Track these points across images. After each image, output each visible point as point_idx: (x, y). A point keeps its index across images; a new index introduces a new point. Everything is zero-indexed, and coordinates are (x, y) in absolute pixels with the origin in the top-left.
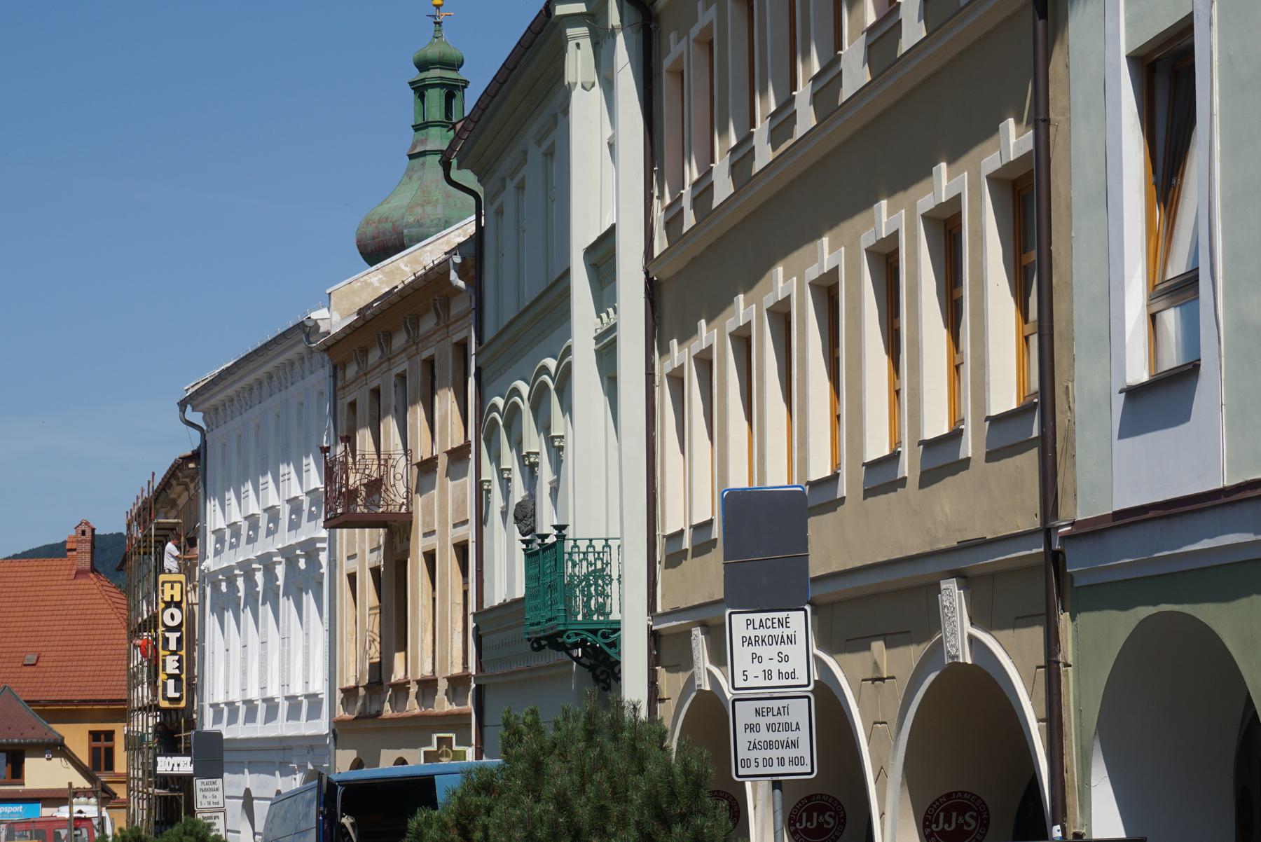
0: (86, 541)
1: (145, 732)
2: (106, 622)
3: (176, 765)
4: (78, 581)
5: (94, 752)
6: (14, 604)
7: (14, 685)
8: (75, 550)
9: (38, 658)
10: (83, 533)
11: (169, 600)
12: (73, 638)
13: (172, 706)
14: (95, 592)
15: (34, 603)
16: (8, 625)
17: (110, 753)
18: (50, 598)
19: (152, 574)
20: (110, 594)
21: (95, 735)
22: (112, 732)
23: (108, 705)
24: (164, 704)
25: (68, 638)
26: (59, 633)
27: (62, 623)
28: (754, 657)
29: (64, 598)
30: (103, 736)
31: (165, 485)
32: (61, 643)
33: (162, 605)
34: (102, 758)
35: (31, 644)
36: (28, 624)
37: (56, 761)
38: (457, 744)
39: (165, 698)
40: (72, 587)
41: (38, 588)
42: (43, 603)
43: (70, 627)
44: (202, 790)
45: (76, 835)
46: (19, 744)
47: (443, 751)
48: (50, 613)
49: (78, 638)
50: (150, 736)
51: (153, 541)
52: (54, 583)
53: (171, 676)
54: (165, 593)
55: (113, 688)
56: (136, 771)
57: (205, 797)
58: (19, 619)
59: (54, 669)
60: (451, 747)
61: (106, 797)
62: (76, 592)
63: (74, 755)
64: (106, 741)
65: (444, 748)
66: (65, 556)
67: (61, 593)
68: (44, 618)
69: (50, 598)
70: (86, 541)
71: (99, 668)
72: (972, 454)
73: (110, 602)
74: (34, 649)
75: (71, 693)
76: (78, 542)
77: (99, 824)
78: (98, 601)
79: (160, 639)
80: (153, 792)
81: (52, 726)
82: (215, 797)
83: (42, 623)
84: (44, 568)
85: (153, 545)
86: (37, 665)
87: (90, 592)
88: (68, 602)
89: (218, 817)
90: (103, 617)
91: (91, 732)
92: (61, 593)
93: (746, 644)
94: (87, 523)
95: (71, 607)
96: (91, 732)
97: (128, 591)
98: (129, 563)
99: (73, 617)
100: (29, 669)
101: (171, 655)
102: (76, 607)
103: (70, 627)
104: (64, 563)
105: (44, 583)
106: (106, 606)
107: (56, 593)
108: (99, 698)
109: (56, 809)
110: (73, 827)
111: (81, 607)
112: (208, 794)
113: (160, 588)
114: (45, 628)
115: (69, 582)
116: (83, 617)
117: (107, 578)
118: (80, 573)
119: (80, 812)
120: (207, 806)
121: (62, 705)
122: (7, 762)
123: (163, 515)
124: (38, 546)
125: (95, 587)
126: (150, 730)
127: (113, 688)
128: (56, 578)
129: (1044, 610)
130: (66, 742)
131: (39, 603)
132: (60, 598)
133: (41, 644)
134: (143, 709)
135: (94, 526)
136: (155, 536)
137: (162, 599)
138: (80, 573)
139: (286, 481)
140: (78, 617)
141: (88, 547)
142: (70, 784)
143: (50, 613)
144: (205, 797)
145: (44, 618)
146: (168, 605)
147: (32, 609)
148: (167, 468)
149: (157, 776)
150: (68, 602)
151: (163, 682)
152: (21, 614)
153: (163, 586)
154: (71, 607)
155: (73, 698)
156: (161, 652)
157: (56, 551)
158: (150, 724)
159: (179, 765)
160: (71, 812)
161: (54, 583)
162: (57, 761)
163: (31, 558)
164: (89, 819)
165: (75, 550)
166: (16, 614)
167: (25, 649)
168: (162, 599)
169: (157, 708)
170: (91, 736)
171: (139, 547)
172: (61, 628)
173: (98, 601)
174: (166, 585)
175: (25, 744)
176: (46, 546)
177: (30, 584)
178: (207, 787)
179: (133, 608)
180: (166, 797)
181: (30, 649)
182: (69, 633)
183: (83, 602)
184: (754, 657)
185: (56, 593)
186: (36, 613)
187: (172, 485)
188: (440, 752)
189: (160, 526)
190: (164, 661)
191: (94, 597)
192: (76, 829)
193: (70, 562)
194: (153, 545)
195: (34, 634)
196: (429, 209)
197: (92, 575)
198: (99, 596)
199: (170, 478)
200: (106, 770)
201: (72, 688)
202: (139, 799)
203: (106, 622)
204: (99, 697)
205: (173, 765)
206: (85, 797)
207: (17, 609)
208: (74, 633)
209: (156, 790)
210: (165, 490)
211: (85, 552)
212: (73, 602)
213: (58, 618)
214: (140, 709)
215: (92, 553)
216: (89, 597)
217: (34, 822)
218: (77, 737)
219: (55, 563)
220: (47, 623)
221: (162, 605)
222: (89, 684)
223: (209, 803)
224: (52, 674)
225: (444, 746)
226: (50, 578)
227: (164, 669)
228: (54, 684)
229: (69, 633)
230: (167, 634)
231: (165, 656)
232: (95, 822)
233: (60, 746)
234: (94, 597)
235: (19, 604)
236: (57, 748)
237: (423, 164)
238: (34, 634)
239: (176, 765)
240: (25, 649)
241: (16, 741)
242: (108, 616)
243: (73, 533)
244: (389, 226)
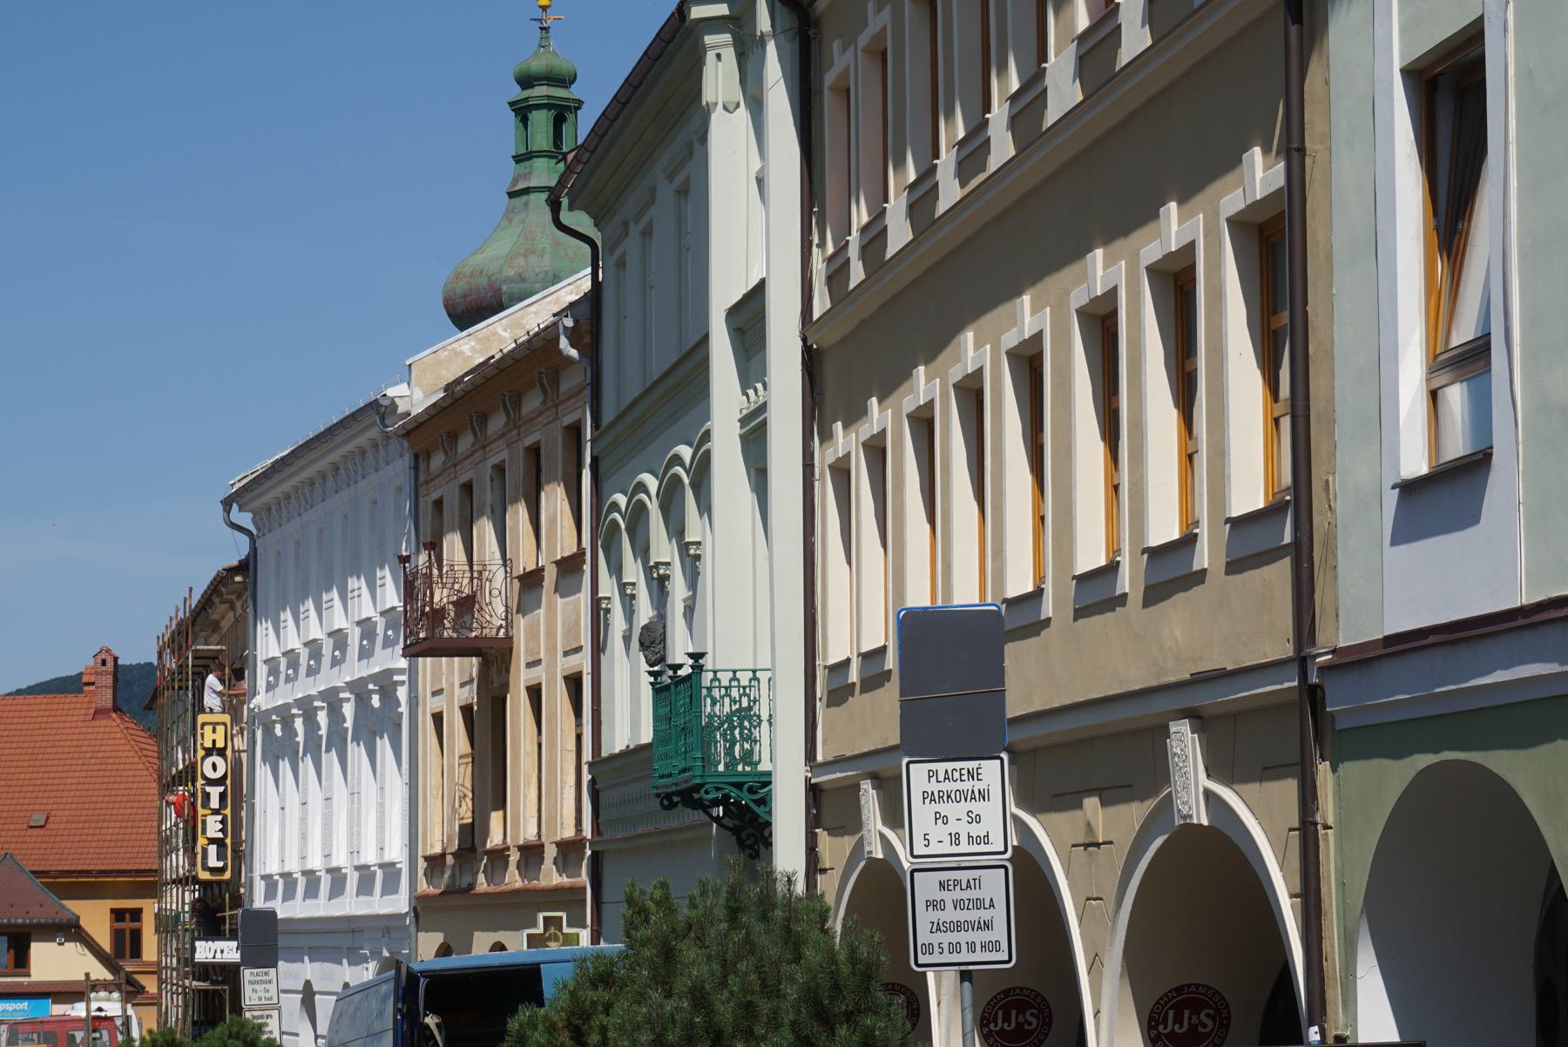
0: (107, 673)
1: (180, 910)
2: (132, 773)
3: (219, 951)
4: (97, 723)
5: (117, 936)
6: (18, 751)
7: (17, 852)
8: (93, 684)
9: (48, 818)
10: (104, 663)
11: (211, 746)
12: (90, 793)
13: (214, 878)
14: (118, 736)
15: (42, 750)
16: (10, 777)
17: (136, 936)
18: (62, 743)
19: (190, 714)
20: (137, 739)
21: (118, 914)
22: (139, 911)
23: (134, 877)
24: (204, 875)
25: (84, 793)
26: (74, 787)
27: (77, 774)
28: (938, 816)
29: (80, 743)
30: (128, 916)
31: (205, 604)
32: (76, 800)
33: (201, 753)
34: (127, 942)
35: (39, 801)
36: (35, 775)
37: (70, 946)
39: (205, 867)
40: (90, 730)
41: (48, 732)
42: (54, 750)
43: (88, 780)
44: (251, 982)
45: (94, 1039)
46: (24, 925)
47: (550, 934)
48: (62, 762)
49: (97, 793)
50: (187, 915)
51: (190, 673)
52: (68, 725)
53: (212, 841)
54: (205, 737)
55: (140, 855)
56: (169, 959)
57: (254, 991)
58: (24, 770)
59: (67, 832)
60: (560, 929)
61: (131, 991)
62: (94, 736)
63: (92, 939)
64: (132, 921)
65: (552, 930)
67: (76, 737)
68: (55, 769)
69: (62, 743)
70: (107, 673)
71: (123, 831)
72: (1209, 564)
73: (137, 749)
74: (43, 807)
75: (88, 861)
76: (97, 673)
77: (123, 1024)
78: (121, 748)
79: (200, 794)
80: (191, 984)
81: (65, 902)
82: (268, 991)
83: (53, 775)
85: (190, 677)
86: (46, 827)
87: (112, 736)
88: (84, 749)
89: (271, 1016)
90: (128, 767)
91: (113, 911)
92: (76, 737)
94: (108, 651)
95: (89, 755)
96: (113, 911)
97: (159, 735)
98: (160, 701)
99: (91, 767)
100: (36, 832)
101: (212, 814)
102: (95, 755)
103: (88, 780)
104: (80, 700)
105: (55, 725)
106: (132, 754)
107: (70, 737)
108: (123, 867)
109: (69, 1006)
110: (91, 1028)
111: (101, 755)
112: (259, 987)
113: (199, 731)
114: (56, 781)
115: (86, 724)
116: (103, 767)
117: (133, 718)
118: (99, 713)
119: (100, 1009)
120: (257, 1002)
121: (77, 877)
123: (203, 641)
124: (48, 679)
125: (118, 730)
126: (187, 908)
127: (140, 855)
128: (69, 719)
129: (1298, 759)
130: (82, 923)
131: (48, 750)
132: (74, 743)
133: (52, 801)
134: (178, 882)
135: (117, 655)
136: (192, 666)
137: (202, 744)
138: (99, 713)
140: (97, 767)
141: (109, 680)
142: (87, 975)
143: (62, 762)
144: (254, 991)
145: (55, 769)
146: (209, 752)
147: (40, 757)
148: (208, 582)
149: (195, 965)
150: (84, 749)
151: (202, 847)
152: (26, 764)
153: (202, 729)
154: (89, 755)
155: (91, 868)
156: (201, 811)
157: (69, 685)
158: (187, 901)
159: (222, 952)
160: (88, 1010)
161: (68, 725)
162: (71, 947)
163: (38, 694)
164: (111, 1019)
165: (93, 684)
166: (20, 764)
167: (31, 807)
168: (202, 744)
169: (195, 880)
170: (114, 916)
171: (173, 680)
172: (76, 781)
173: (121, 748)
174: (206, 727)
175: (32, 926)
176: (57, 679)
177: (38, 726)
178: (258, 978)
179: (166, 756)
180: (206, 992)
181: (37, 807)
182: (86, 787)
183: (103, 748)
184: (938, 816)
185: (70, 737)
186: (44, 763)
187: (213, 603)
188: (547, 935)
189: (198, 654)
190: (204, 822)
191: (117, 742)
192: (94, 1031)
193: (86, 699)
194: (190, 677)
195: (43, 788)
197: (114, 715)
198: (123, 741)
199: (211, 594)
200: (132, 957)
201: (90, 856)
202: (173, 994)
203: (132, 773)
204: (123, 867)
205: (216, 951)
206: (105, 991)
207: (21, 757)
208: (92, 787)
209: (194, 983)
210: (205, 610)
211: (106, 687)
212: (90, 749)
213: (73, 768)
214: (174, 882)
215: (115, 688)
217: (42, 1022)
218: (95, 917)
219: (68, 700)
220: (59, 775)
221: (201, 753)
222: (111, 850)
223: (260, 999)
224: (65, 838)
225: (553, 928)
226: (62, 719)
227: (204, 831)
228: (67, 851)
229: (86, 787)
230: (208, 789)
231: (206, 816)
232: (119, 1022)
233: (75, 928)
234: (117, 742)
235: (24, 751)
236: (71, 930)
237: (526, 204)
238: (43, 788)
239: (219, 951)
240: (31, 807)
241: (20, 921)
242: (134, 767)
243: (91, 662)
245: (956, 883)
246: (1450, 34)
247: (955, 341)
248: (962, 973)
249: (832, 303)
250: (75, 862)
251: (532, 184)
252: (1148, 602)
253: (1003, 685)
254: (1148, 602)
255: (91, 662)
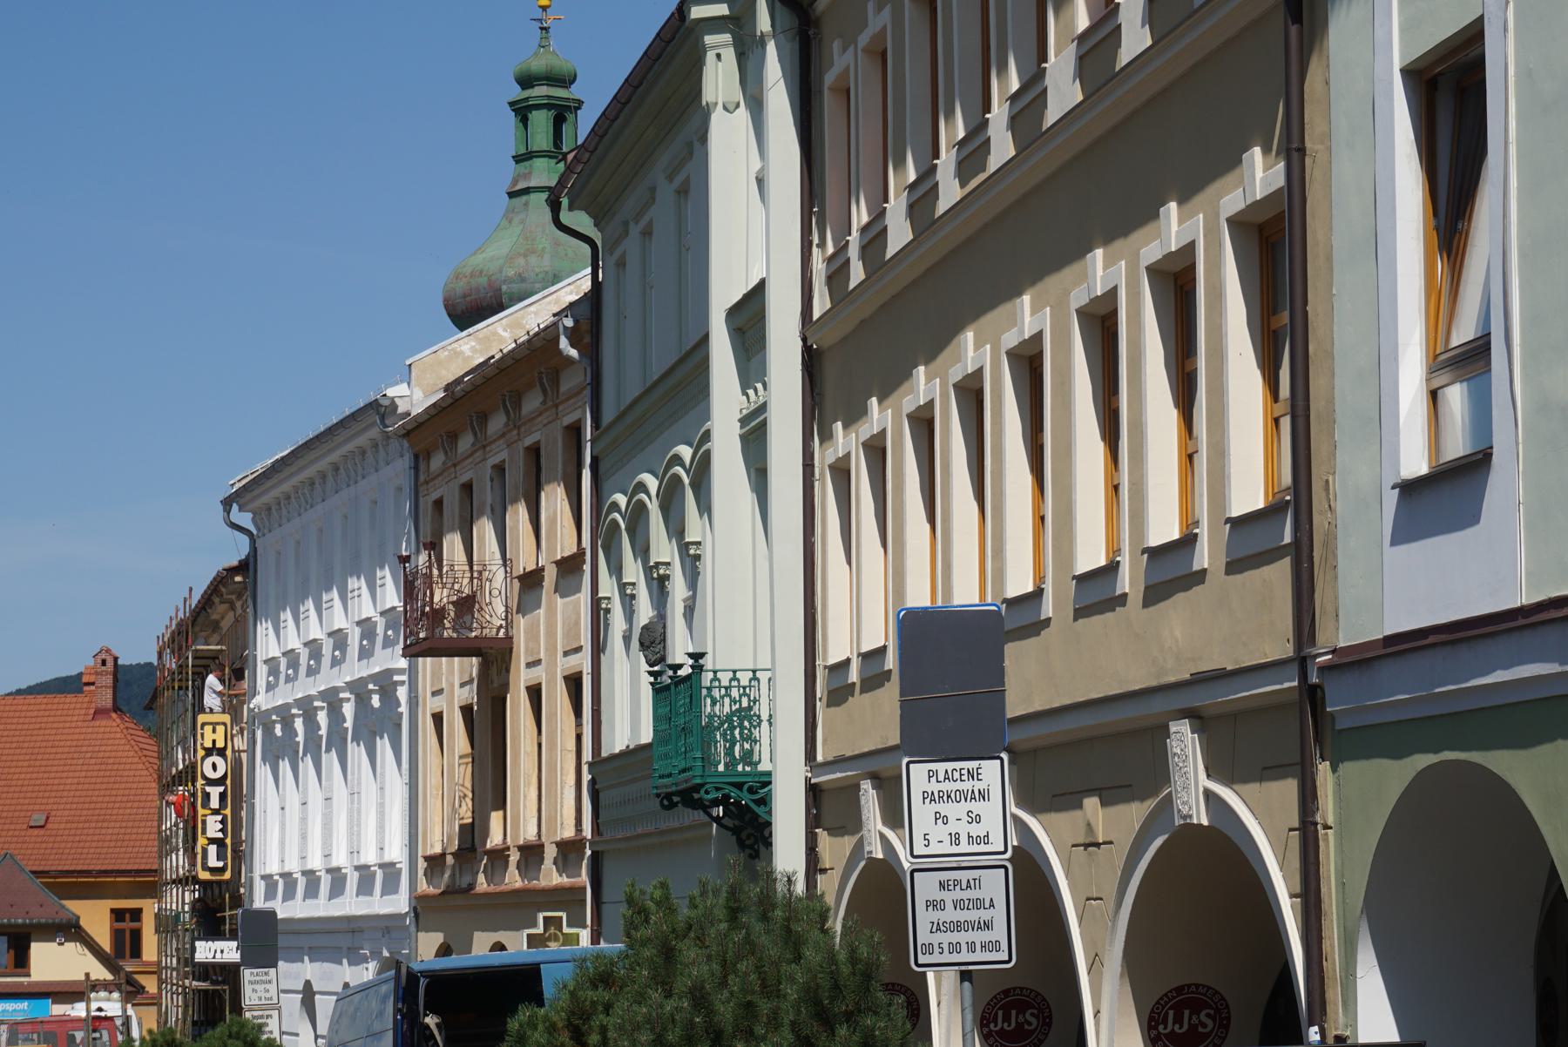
0: (107, 673)
1: (180, 910)
2: (132, 773)
3: (219, 951)
4: (97, 723)
5: (117, 936)
6: (18, 751)
7: (17, 852)
8: (93, 684)
9: (48, 818)
10: (104, 663)
11: (211, 746)
12: (90, 793)
13: (214, 878)
14: (118, 736)
15: (42, 750)
16: (10, 777)
17: (136, 936)
18: (62, 743)
19: (190, 714)
20: (137, 739)
21: (118, 914)
22: (139, 911)
23: (134, 877)
24: (204, 875)
25: (84, 793)
26: (74, 787)
27: (77, 774)
29: (80, 743)
30: (128, 916)
31: (205, 604)
32: (76, 800)
33: (201, 753)
34: (127, 942)
35: (39, 801)
36: (35, 775)
37: (70, 946)
38: (568, 925)
39: (205, 867)
40: (90, 730)
41: (48, 732)
42: (54, 750)
43: (88, 780)
44: (251, 982)
45: (94, 1039)
46: (24, 925)
47: (550, 934)
48: (62, 762)
49: (97, 793)
50: (187, 915)
51: (190, 673)
52: (68, 725)
53: (212, 841)
54: (205, 737)
55: (140, 855)
56: (169, 959)
57: (254, 991)
58: (24, 770)
59: (67, 832)
60: (560, 929)
61: (131, 991)
62: (94, 736)
63: (92, 939)
64: (132, 921)
65: (552, 930)
66: (81, 691)
67: (76, 737)
68: (55, 769)
69: (62, 743)
70: (107, 673)
71: (123, 831)
73: (137, 749)
74: (43, 807)
75: (88, 861)
76: (97, 673)
77: (123, 1024)
78: (121, 748)
79: (200, 794)
80: (191, 984)
81: (65, 902)
82: (268, 991)
83: (53, 775)
84: (55, 707)
85: (190, 677)
86: (46, 827)
87: (112, 736)
88: (84, 749)
89: (271, 1016)
90: (128, 767)
91: (113, 911)
92: (76, 737)
93: (927, 801)
94: (108, 651)
95: (89, 755)
96: (113, 911)
97: (159, 735)
98: (160, 701)
99: (91, 767)
100: (36, 832)
101: (212, 814)
102: (95, 755)
103: (88, 780)
104: (80, 700)
105: (55, 725)
106: (132, 754)
107: (70, 737)
108: (123, 867)
109: (69, 1006)
110: (91, 1028)
111: (101, 755)
112: (259, 987)
113: (199, 731)
114: (56, 781)
115: (86, 724)
116: (103, 767)
117: (133, 718)
118: (99, 713)
119: (100, 1009)
120: (257, 1002)
121: (77, 877)
122: (9, 948)
123: (203, 641)
124: (48, 679)
125: (118, 730)
126: (187, 908)
127: (140, 855)
128: (69, 719)
129: (1298, 759)
130: (82, 923)
131: (48, 750)
132: (74, 743)
133: (52, 801)
134: (178, 882)
135: (117, 655)
136: (192, 666)
137: (202, 744)
138: (99, 713)
139: (356, 598)
140: (97, 767)
141: (109, 680)
142: (87, 975)
143: (62, 762)
144: (254, 991)
145: (55, 769)
146: (209, 752)
147: (40, 757)
148: (208, 582)
149: (195, 965)
150: (84, 749)
151: (202, 847)
152: (26, 764)
153: (202, 729)
154: (89, 755)
155: (91, 868)
156: (201, 811)
157: (69, 685)
158: (187, 901)
159: (222, 952)
160: (88, 1010)
161: (68, 725)
162: (71, 947)
163: (38, 694)
164: (111, 1019)
165: (93, 684)
166: (20, 764)
167: (31, 807)
168: (202, 744)
169: (195, 880)
170: (114, 916)
171: (173, 680)
172: (76, 781)
173: (121, 748)
174: (206, 727)
175: (32, 926)
176: (57, 679)
177: (38, 726)
178: (258, 978)
179: (166, 756)
180: (206, 992)
181: (37, 807)
182: (86, 787)
183: (103, 748)
185: (70, 737)
186: (44, 763)
187: (213, 603)
188: (547, 935)
189: (198, 654)
190: (204, 822)
191: (117, 742)
192: (94, 1031)
193: (86, 699)
194: (190, 677)
195: (43, 788)
196: (533, 260)
197: (114, 715)
198: (123, 741)
199: (211, 594)
200: (132, 957)
201: (90, 856)
202: (173, 994)
203: (132, 773)
204: (123, 867)
205: (216, 951)
206: (105, 991)
207: (21, 757)
208: (92, 787)
209: (194, 983)
210: (205, 610)
211: (106, 687)
212: (90, 749)
213: (73, 768)
214: (174, 882)
215: (115, 688)
217: (42, 1022)
218: (95, 917)
219: (68, 700)
220: (59, 775)
221: (201, 753)
222: (111, 850)
223: (260, 999)
224: (65, 838)
225: (553, 928)
226: (62, 719)
227: (204, 831)
228: (67, 851)
229: (86, 787)
230: (208, 789)
231: (206, 816)
232: (119, 1022)
233: (75, 928)
234: (117, 742)
235: (24, 751)
236: (71, 930)
237: (526, 204)
238: (43, 788)
239: (219, 951)
240: (31, 807)
241: (20, 921)
242: (134, 767)
243: (91, 662)
244: (483, 281)
245: (956, 883)
246: (1450, 34)
249: (832, 303)
250: (75, 862)
251: (532, 184)
252: (1148, 602)
253: (1003, 685)
254: (1148, 602)
255: (91, 662)
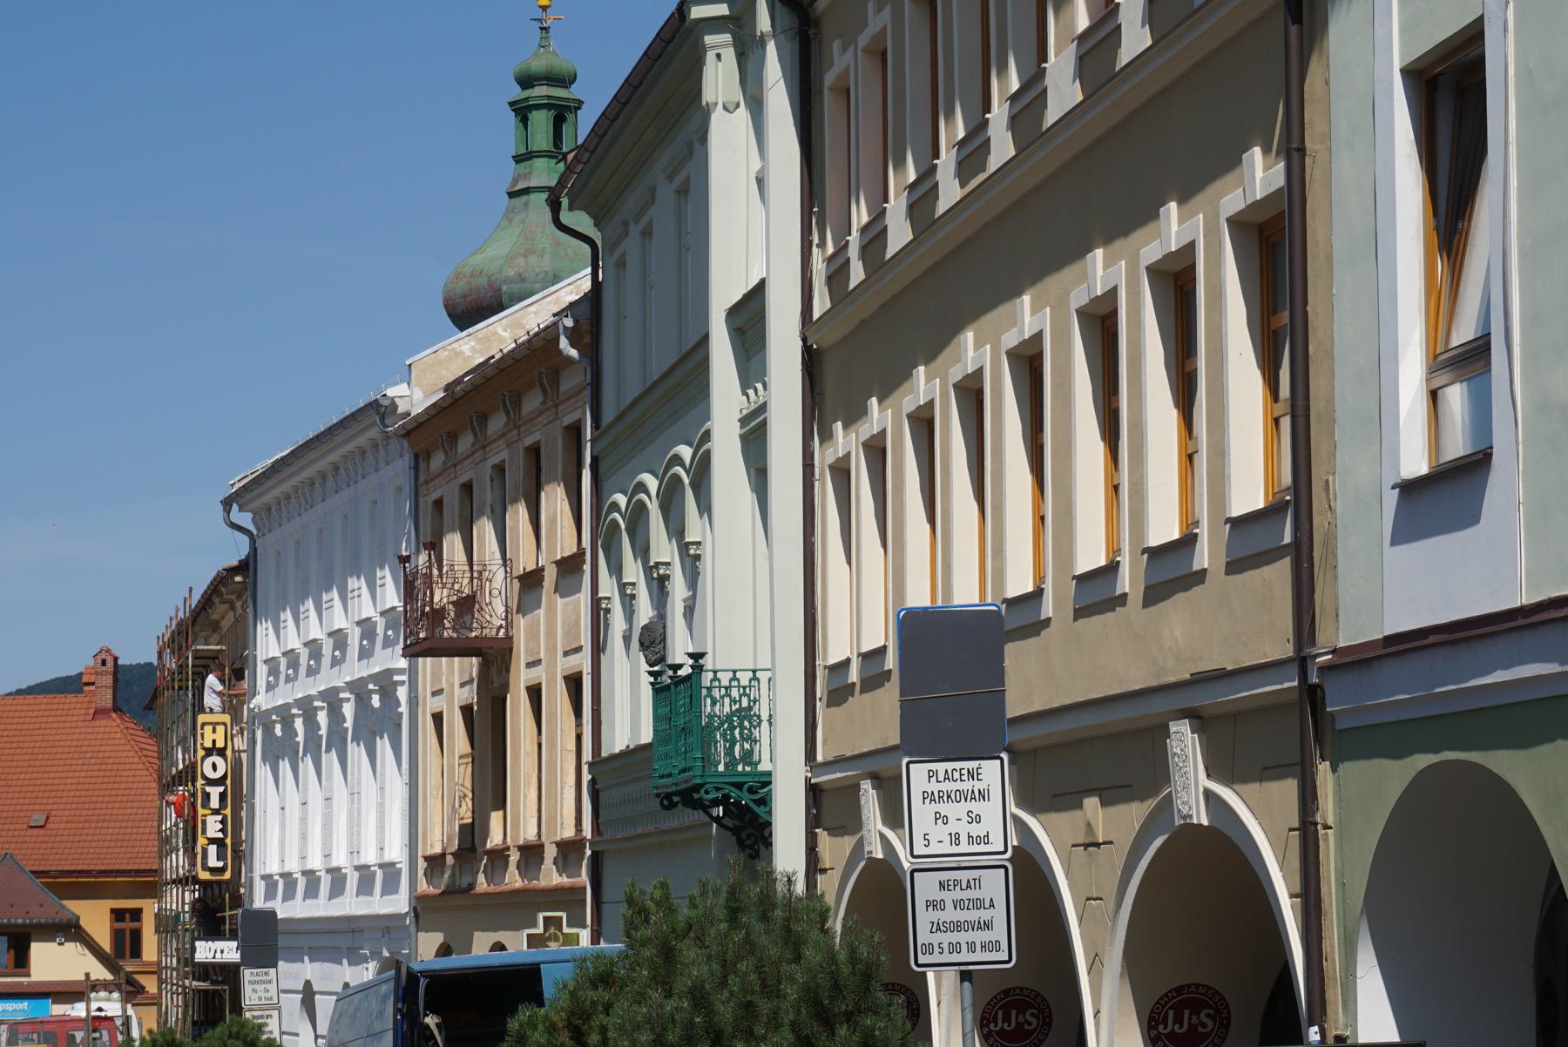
0: (107, 673)
1: (180, 910)
2: (132, 773)
4: (97, 723)
5: (117, 936)
6: (18, 751)
7: (17, 852)
8: (93, 684)
9: (48, 818)
10: (104, 663)
11: (211, 746)
12: (90, 793)
13: (214, 878)
14: (118, 736)
15: (42, 750)
16: (10, 777)
17: (136, 936)
18: (62, 743)
19: (190, 714)
20: (137, 739)
21: (118, 914)
22: (139, 911)
23: (134, 877)
24: (204, 875)
25: (84, 793)
26: (74, 787)
27: (77, 774)
28: (938, 816)
29: (80, 743)
30: (128, 916)
31: (205, 604)
32: (76, 800)
33: (201, 753)
34: (127, 942)
35: (39, 801)
37: (70, 946)
39: (205, 867)
40: (90, 730)
41: (48, 732)
42: (54, 750)
43: (88, 780)
44: (251, 982)
45: (94, 1039)
46: (24, 925)
47: (550, 934)
48: (62, 762)
49: (97, 793)
50: (187, 915)
51: (190, 673)
52: (68, 725)
53: (212, 841)
54: (205, 737)
55: (140, 855)
56: (169, 959)
57: (254, 991)
58: (24, 770)
59: (67, 832)
60: (560, 929)
61: (131, 991)
62: (94, 736)
63: (92, 939)
64: (132, 921)
65: (552, 930)
67: (76, 737)
68: (55, 769)
69: (62, 743)
70: (107, 673)
71: (123, 831)
73: (137, 749)
74: (43, 807)
75: (88, 861)
76: (97, 673)
77: (123, 1024)
78: (121, 748)
79: (200, 794)
80: (191, 984)
81: (65, 902)
82: (268, 991)
83: (53, 775)
85: (190, 677)
86: (46, 827)
87: (112, 736)
88: (84, 749)
89: (271, 1016)
90: (128, 767)
91: (113, 911)
92: (76, 737)
93: (927, 801)
94: (108, 651)
95: (89, 755)
96: (113, 911)
97: (159, 735)
98: (160, 701)
99: (91, 767)
100: (36, 832)
101: (212, 814)
102: (95, 755)
103: (88, 780)
104: (80, 700)
105: (55, 725)
106: (132, 754)
107: (70, 737)
108: (123, 867)
109: (69, 1006)
110: (91, 1028)
111: (101, 755)
112: (259, 987)
113: (199, 731)
114: (56, 781)
115: (86, 724)
116: (103, 767)
117: (133, 718)
118: (99, 713)
119: (100, 1009)
120: (257, 1002)
121: (77, 877)
122: (9, 948)
123: (203, 641)
124: (48, 679)
125: (118, 730)
126: (187, 908)
127: (140, 855)
128: (69, 719)
129: (1298, 759)
130: (82, 923)
131: (48, 750)
132: (74, 743)
133: (52, 801)
134: (178, 882)
135: (117, 655)
136: (192, 666)
137: (202, 744)
138: (99, 713)
140: (97, 767)
141: (109, 680)
142: (87, 975)
143: (62, 762)
144: (254, 991)
145: (55, 769)
147: (40, 757)
148: (208, 582)
149: (195, 965)
150: (84, 749)
151: (202, 847)
152: (26, 764)
153: (202, 729)
154: (89, 755)
155: (91, 868)
156: (201, 811)
157: (69, 685)
158: (187, 901)
160: (88, 1010)
161: (68, 725)
162: (71, 947)
163: (38, 694)
164: (111, 1019)
165: (93, 684)
166: (20, 764)
167: (31, 807)
168: (202, 744)
169: (195, 880)
170: (114, 916)
171: (173, 680)
172: (76, 781)
173: (121, 748)
174: (206, 727)
175: (32, 926)
176: (57, 679)
177: (38, 726)
178: (258, 978)
179: (166, 756)
180: (206, 992)
181: (37, 807)
182: (86, 787)
183: (103, 748)
184: (938, 816)
185: (70, 737)
186: (44, 763)
187: (213, 603)
188: (547, 935)
189: (198, 654)
190: (204, 822)
191: (117, 742)
192: (94, 1031)
193: (86, 699)
194: (190, 677)
195: (43, 788)
196: (533, 260)
197: (114, 715)
198: (123, 741)
199: (211, 594)
200: (132, 957)
201: (90, 856)
202: (173, 994)
203: (132, 773)
204: (123, 867)
205: (216, 951)
206: (105, 991)
207: (21, 757)
208: (92, 787)
209: (194, 983)
210: (205, 610)
211: (106, 687)
212: (90, 749)
213: (73, 768)
214: (174, 882)
215: (115, 688)
216: (110, 742)
217: (42, 1022)
218: (95, 917)
219: (68, 700)
220: (59, 775)
221: (201, 753)
222: (111, 850)
223: (260, 999)
224: (65, 838)
225: (553, 928)
226: (62, 719)
228: (67, 851)
229: (86, 787)
230: (208, 789)
231: (206, 816)
232: (119, 1022)
233: (75, 928)
234: (117, 742)
235: (24, 751)
236: (71, 930)
238: (43, 788)
240: (31, 807)
241: (20, 921)
242: (134, 767)
243: (91, 662)
244: (483, 281)
245: (956, 883)
247: (955, 341)
248: (962, 973)
252: (1148, 602)
254: (1148, 602)
255: (91, 662)
